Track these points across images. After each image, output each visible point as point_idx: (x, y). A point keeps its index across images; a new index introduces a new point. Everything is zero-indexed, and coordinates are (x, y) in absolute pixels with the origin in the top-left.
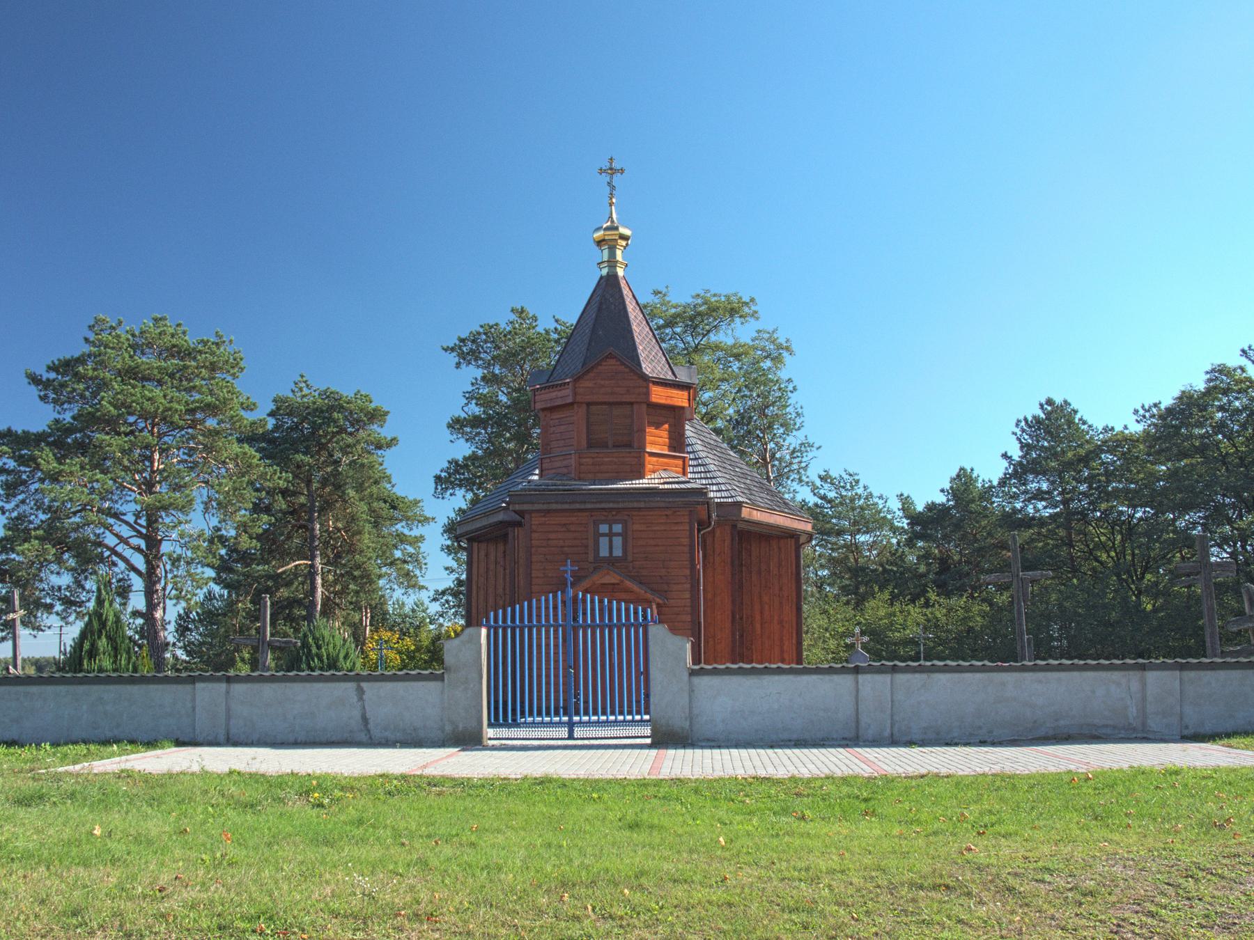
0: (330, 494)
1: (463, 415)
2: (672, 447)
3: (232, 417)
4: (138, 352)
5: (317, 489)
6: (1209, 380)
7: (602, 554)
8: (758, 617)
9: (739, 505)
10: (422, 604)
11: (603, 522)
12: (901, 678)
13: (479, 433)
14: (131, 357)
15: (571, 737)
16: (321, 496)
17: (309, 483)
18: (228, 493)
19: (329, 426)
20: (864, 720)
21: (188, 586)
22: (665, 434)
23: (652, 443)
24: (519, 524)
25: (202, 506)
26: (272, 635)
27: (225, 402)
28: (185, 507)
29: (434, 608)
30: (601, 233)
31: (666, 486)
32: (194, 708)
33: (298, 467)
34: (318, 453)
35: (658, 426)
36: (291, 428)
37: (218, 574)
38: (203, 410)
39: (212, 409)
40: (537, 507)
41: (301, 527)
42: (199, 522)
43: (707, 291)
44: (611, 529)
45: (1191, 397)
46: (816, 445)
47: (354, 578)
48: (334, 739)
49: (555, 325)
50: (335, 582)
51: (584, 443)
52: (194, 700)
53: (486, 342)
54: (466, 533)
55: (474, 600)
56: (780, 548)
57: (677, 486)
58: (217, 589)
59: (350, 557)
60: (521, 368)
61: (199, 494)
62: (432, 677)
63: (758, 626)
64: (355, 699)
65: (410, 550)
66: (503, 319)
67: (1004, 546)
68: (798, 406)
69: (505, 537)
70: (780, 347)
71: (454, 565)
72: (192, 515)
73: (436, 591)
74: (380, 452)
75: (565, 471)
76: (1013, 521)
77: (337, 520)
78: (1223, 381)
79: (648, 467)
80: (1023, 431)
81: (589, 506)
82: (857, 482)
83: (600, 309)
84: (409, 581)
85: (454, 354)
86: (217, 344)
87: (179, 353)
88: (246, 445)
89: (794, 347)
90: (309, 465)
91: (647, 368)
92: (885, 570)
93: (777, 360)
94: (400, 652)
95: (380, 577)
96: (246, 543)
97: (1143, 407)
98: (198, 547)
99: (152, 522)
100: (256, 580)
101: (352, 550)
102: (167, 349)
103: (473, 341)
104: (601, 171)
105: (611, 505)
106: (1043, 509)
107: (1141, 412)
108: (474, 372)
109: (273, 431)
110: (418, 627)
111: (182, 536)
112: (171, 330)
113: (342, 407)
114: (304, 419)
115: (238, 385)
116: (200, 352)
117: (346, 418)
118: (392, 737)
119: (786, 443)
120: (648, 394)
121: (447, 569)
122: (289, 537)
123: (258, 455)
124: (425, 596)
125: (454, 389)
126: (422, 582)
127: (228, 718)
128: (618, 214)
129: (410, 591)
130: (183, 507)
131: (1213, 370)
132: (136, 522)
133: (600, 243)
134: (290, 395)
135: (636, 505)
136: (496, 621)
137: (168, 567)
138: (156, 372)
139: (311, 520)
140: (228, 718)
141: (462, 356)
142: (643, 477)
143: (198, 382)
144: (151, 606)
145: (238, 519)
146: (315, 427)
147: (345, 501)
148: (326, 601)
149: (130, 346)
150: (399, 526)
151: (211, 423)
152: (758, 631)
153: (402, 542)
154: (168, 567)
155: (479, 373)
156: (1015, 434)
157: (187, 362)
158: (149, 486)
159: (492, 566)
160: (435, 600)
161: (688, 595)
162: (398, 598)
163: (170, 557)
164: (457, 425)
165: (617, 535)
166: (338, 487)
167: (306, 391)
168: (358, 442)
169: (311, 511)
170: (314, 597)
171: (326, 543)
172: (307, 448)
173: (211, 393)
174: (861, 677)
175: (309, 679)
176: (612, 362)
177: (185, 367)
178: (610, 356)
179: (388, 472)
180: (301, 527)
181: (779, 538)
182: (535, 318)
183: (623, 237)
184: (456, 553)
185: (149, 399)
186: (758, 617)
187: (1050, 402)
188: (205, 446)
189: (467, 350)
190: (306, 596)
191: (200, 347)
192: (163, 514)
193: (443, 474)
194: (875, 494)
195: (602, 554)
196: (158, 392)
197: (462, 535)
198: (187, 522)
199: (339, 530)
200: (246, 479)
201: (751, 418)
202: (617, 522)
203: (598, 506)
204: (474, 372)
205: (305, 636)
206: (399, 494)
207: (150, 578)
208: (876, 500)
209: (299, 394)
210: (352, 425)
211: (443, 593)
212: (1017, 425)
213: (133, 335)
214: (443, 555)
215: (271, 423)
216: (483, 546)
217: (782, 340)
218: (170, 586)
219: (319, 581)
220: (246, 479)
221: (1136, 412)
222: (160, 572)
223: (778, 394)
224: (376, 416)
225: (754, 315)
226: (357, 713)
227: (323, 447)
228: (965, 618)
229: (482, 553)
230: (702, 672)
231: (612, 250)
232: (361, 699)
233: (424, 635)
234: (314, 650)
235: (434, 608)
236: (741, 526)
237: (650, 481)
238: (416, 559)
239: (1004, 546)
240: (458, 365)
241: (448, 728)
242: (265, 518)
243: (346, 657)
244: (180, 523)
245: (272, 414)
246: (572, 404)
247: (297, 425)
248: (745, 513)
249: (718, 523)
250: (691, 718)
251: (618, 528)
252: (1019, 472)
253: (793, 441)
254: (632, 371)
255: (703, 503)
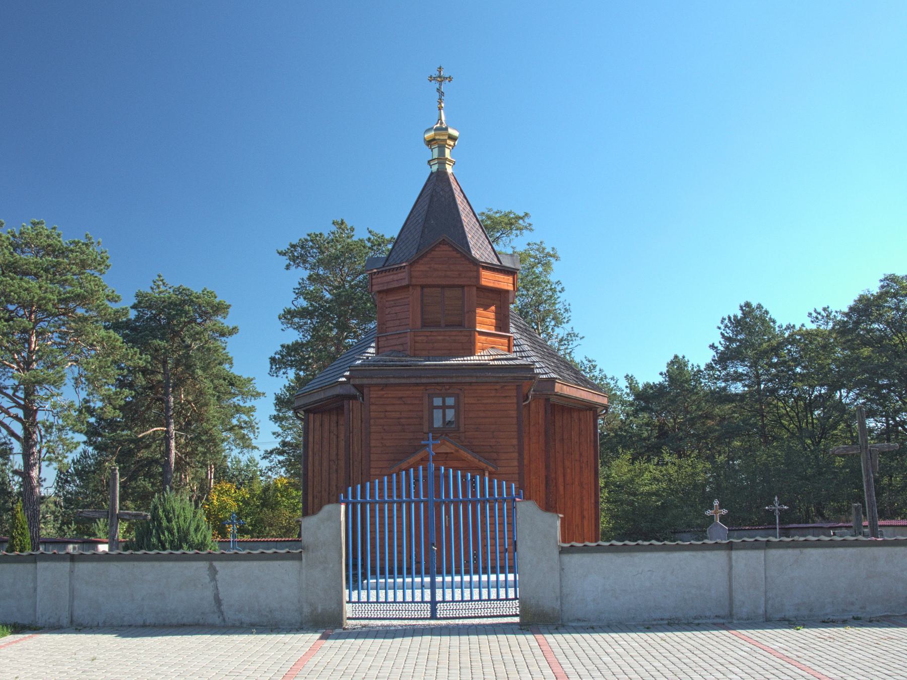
0: (182, 373)
1: (293, 308)
2: (498, 328)
3: (99, 306)
4: (19, 250)
5: (172, 368)
6: (882, 287)
7: (435, 426)
8: (561, 480)
9: (553, 380)
10: (254, 461)
11: (438, 395)
12: (774, 553)
13: (306, 323)
14: (11, 253)
15: (433, 617)
16: (174, 375)
17: (165, 363)
18: (95, 371)
19: (181, 317)
20: (738, 597)
21: (60, 449)
22: (492, 315)
23: (482, 323)
24: (354, 397)
25: (73, 381)
26: (121, 509)
27: (92, 293)
28: (57, 382)
29: (264, 464)
30: (433, 133)
31: (496, 363)
32: (35, 590)
33: (156, 350)
34: (172, 339)
35: (486, 307)
36: (150, 318)
37: (89, 438)
38: (74, 301)
39: (81, 299)
40: (374, 381)
41: (158, 399)
42: (70, 395)
43: (490, 210)
44: (444, 402)
45: (869, 299)
46: (580, 336)
47: (202, 442)
48: (185, 621)
49: (369, 235)
50: (187, 445)
51: (419, 323)
52: (35, 580)
53: (312, 247)
54: (305, 405)
55: (310, 468)
56: (580, 420)
57: (506, 362)
58: (90, 449)
59: (199, 424)
60: (341, 270)
61: (70, 371)
62: (289, 557)
63: (561, 488)
64: (208, 579)
65: (244, 417)
66: (326, 229)
67: (708, 416)
68: (566, 303)
69: (339, 410)
70: (548, 255)
71: (280, 430)
72: (63, 388)
73: (266, 451)
74: (223, 339)
75: (401, 348)
76: (722, 397)
77: (188, 394)
78: (894, 287)
79: (479, 345)
80: (726, 326)
81: (424, 381)
82: (595, 367)
83: (431, 201)
84: (245, 443)
85: (285, 258)
86: (87, 245)
87: (54, 251)
88: (111, 331)
89: (559, 254)
90: (165, 348)
91: (476, 253)
92: (616, 435)
93: (547, 265)
94: (237, 501)
95: (223, 441)
96: (110, 413)
97: (815, 311)
98: (68, 417)
99: (29, 393)
100: (120, 443)
101: (200, 418)
102: (43, 248)
103: (302, 247)
104: (431, 79)
105: (445, 380)
106: (738, 388)
107: (814, 314)
108: (303, 273)
109: (135, 321)
110: (252, 478)
111: (54, 406)
112: (47, 232)
113: (192, 301)
114: (161, 311)
115: (104, 279)
116: (72, 251)
117: (195, 311)
118: (246, 620)
119: (555, 333)
120: (478, 277)
121: (274, 434)
122: (149, 408)
123: (121, 339)
124: (257, 455)
125: (286, 286)
126: (254, 442)
127: (72, 597)
128: (446, 116)
129: (245, 451)
130: (55, 382)
131: (886, 279)
132: (14, 394)
133: (429, 142)
134: (150, 291)
135: (468, 380)
136: (354, 496)
137: (43, 433)
138: (32, 267)
139: (166, 394)
140: (72, 597)
141: (293, 259)
142: (473, 355)
143: (69, 276)
144: (28, 466)
145: (104, 392)
146: (170, 318)
147: (194, 378)
148: (179, 461)
149: (11, 244)
150: (235, 400)
151: (80, 312)
152: (562, 492)
153: (238, 411)
154: (43, 433)
155: (305, 273)
156: (719, 328)
157: (58, 260)
158: (27, 364)
159: (326, 435)
160: (264, 458)
161: (516, 463)
162: (235, 456)
163: (44, 425)
164: (289, 316)
165: (450, 407)
166: (189, 367)
167: (162, 288)
168: (205, 329)
169: (166, 387)
170: (168, 457)
171: (179, 414)
172: (163, 334)
173: (81, 285)
174: (734, 554)
175: (158, 558)
176: (446, 248)
177: (59, 263)
178: (444, 242)
179: (230, 355)
180: (158, 399)
181: (579, 410)
182: (352, 229)
183: (453, 138)
184: (281, 422)
185: (26, 289)
186: (561, 480)
187: (748, 305)
188: (76, 331)
189: (297, 254)
190: (162, 457)
191: (72, 247)
192: (38, 388)
193: (277, 356)
194: (609, 376)
195: (435, 426)
196: (34, 284)
197: (299, 407)
198: (58, 395)
199: (190, 403)
200: (111, 359)
201: (527, 312)
202: (450, 395)
203: (433, 380)
204: (303, 273)
205: (156, 508)
206: (236, 374)
207: (27, 442)
208: (609, 381)
209: (157, 291)
210: (201, 316)
211: (271, 452)
212: (722, 322)
213: (14, 236)
214: (272, 423)
215: (133, 314)
216: (318, 416)
217: (548, 250)
218: (44, 451)
219: (173, 444)
220: (111, 359)
221: (810, 314)
222: (36, 437)
223: (550, 293)
224: (220, 309)
225: (529, 227)
226: (209, 594)
227: (176, 334)
228: (693, 473)
229: (318, 423)
230: (572, 550)
231: (442, 149)
232: (213, 579)
233: (255, 486)
234: (165, 523)
235: (264, 464)
236: (553, 399)
237: (480, 357)
238: (250, 426)
239: (708, 416)
240: (288, 267)
241: (307, 610)
242: (126, 391)
243: (197, 529)
244: (52, 395)
245: (134, 307)
246: (407, 287)
247: (155, 316)
248: (558, 388)
249: (534, 396)
250: (562, 597)
251: (450, 401)
252: (724, 358)
253: (561, 332)
254: (464, 256)
255: (531, 378)
